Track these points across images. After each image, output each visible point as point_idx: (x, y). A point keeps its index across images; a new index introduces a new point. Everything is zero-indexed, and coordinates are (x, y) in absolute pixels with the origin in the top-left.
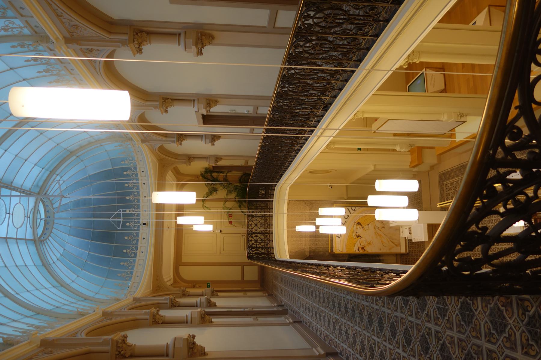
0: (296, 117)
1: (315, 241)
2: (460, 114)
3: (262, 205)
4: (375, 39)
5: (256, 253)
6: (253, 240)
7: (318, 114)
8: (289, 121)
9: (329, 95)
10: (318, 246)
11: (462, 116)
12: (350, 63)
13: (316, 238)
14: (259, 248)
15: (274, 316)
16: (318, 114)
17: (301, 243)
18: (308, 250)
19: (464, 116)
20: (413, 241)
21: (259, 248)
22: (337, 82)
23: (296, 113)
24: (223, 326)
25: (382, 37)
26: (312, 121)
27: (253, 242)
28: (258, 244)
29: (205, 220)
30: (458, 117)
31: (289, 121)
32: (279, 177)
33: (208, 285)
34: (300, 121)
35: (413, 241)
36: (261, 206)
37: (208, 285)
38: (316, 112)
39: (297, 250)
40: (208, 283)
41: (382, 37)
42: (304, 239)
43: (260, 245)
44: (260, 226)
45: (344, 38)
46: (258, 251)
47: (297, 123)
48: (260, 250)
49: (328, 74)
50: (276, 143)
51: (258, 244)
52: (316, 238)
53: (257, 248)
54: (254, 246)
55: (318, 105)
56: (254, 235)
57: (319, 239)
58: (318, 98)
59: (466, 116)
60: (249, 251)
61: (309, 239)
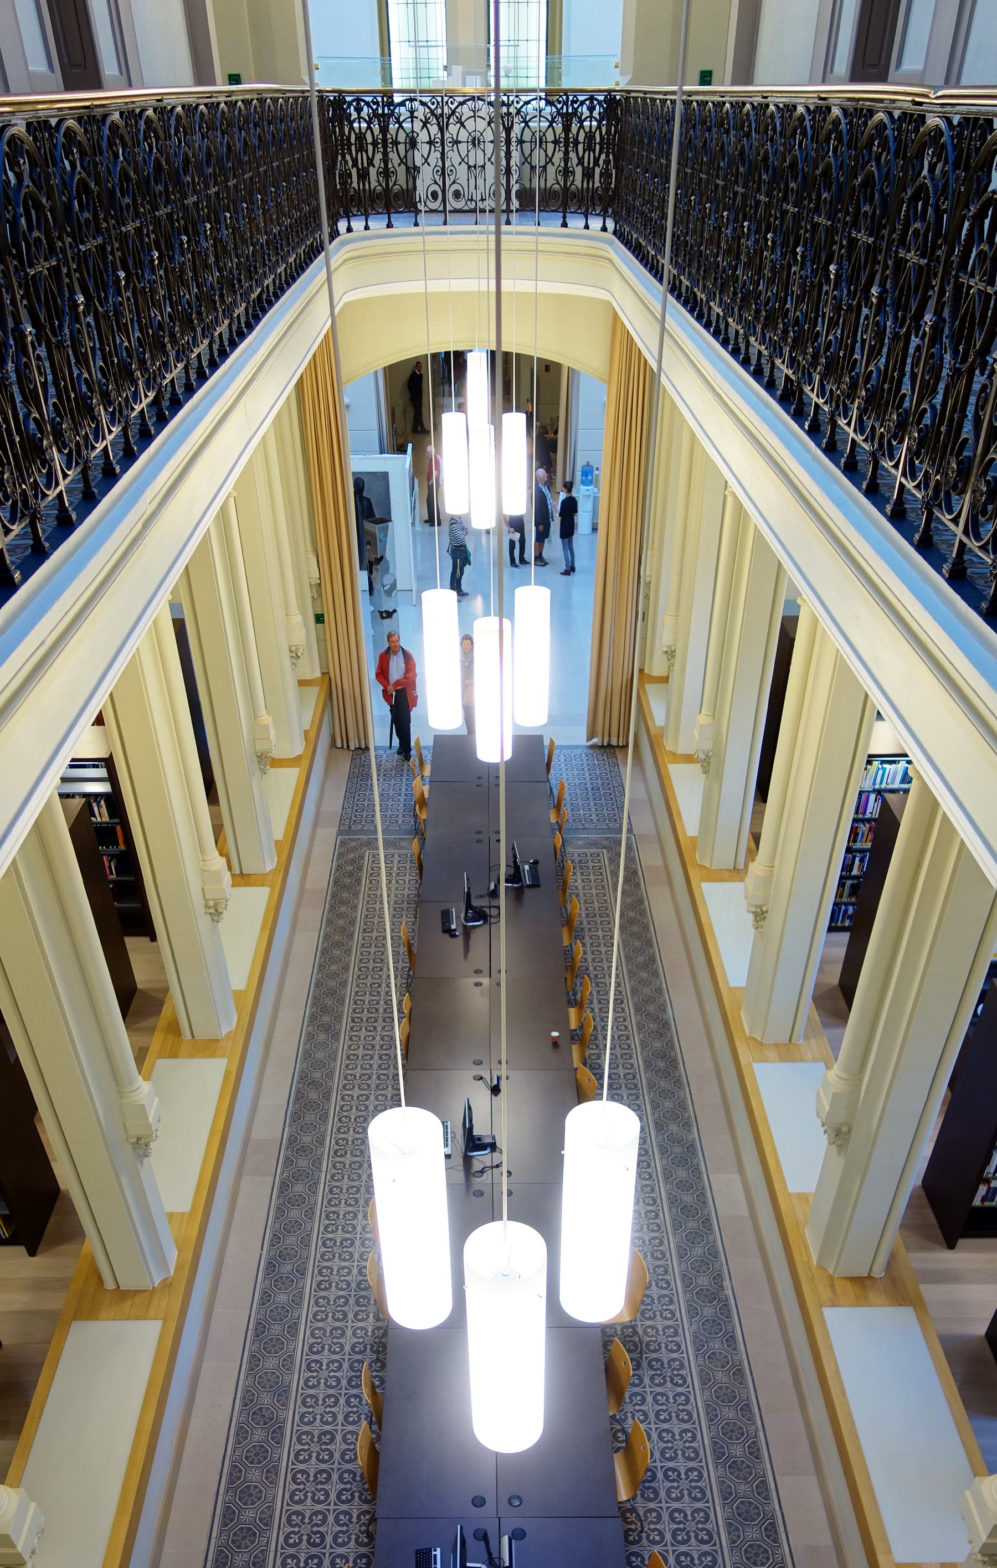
0: (955, 352)
2: (763, 913)
3: (551, 170)
4: (946, 568)
5: (361, 137)
7: (946, 518)
8: (942, 292)
9: (978, 537)
11: (756, 917)
12: (957, 524)
14: (386, 160)
16: (946, 518)
19: (757, 922)
21: (386, 160)
22: (962, 521)
23: (920, 315)
24: (132, 1497)
25: (915, 566)
26: (911, 472)
28: (401, 148)
30: (757, 906)
31: (942, 292)
32: (783, 370)
34: (924, 385)
36: (549, 166)
38: (956, 509)
41: (915, 566)
43: (396, 161)
44: (471, 163)
45: (981, 413)
46: (370, 148)
47: (915, 364)
49: (938, 407)
50: (912, 257)
55: (877, 419)
56: (434, 129)
58: (970, 460)
59: (757, 928)
60: (367, 104)
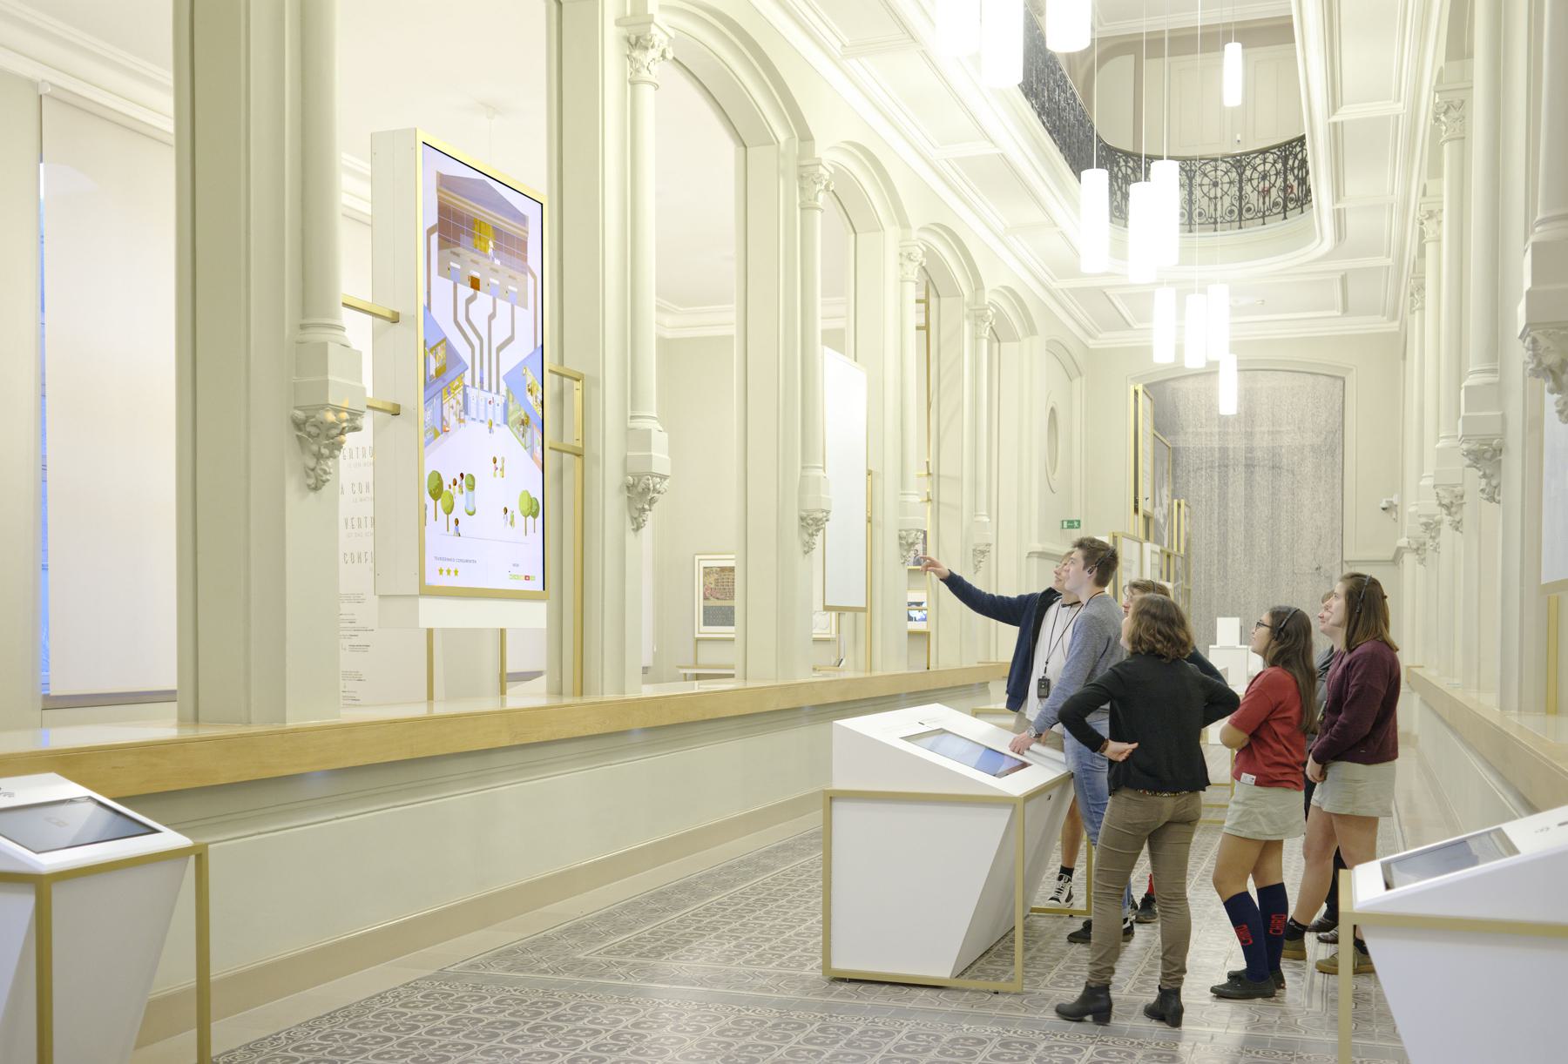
1: (1209, 464)
6: (1268, 166)
10: (1192, 474)
13: (1217, 469)
15: (471, 215)
17: (1204, 421)
18: (1181, 444)
20: (1211, 647)
27: (1268, 166)
28: (1296, 171)
29: (1091, 166)
33: (1076, 524)
35: (1211, 647)
37: (1076, 524)
39: (1181, 408)
40: (1079, 522)
42: (1216, 430)
48: (1278, 184)
51: (1296, 171)
52: (1219, 466)
53: (1241, 181)
54: (1248, 173)
57: (1216, 478)
61: (1216, 445)
